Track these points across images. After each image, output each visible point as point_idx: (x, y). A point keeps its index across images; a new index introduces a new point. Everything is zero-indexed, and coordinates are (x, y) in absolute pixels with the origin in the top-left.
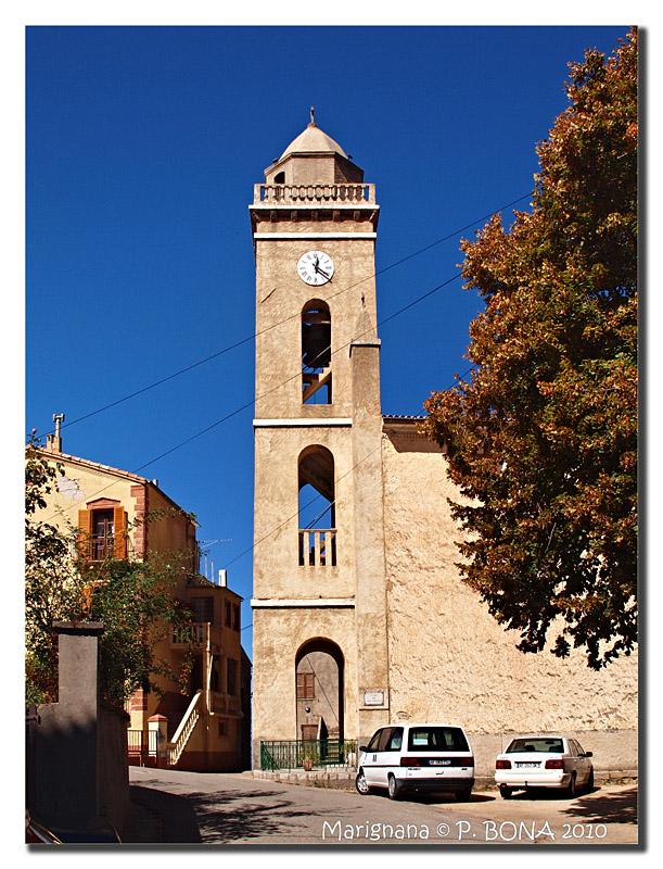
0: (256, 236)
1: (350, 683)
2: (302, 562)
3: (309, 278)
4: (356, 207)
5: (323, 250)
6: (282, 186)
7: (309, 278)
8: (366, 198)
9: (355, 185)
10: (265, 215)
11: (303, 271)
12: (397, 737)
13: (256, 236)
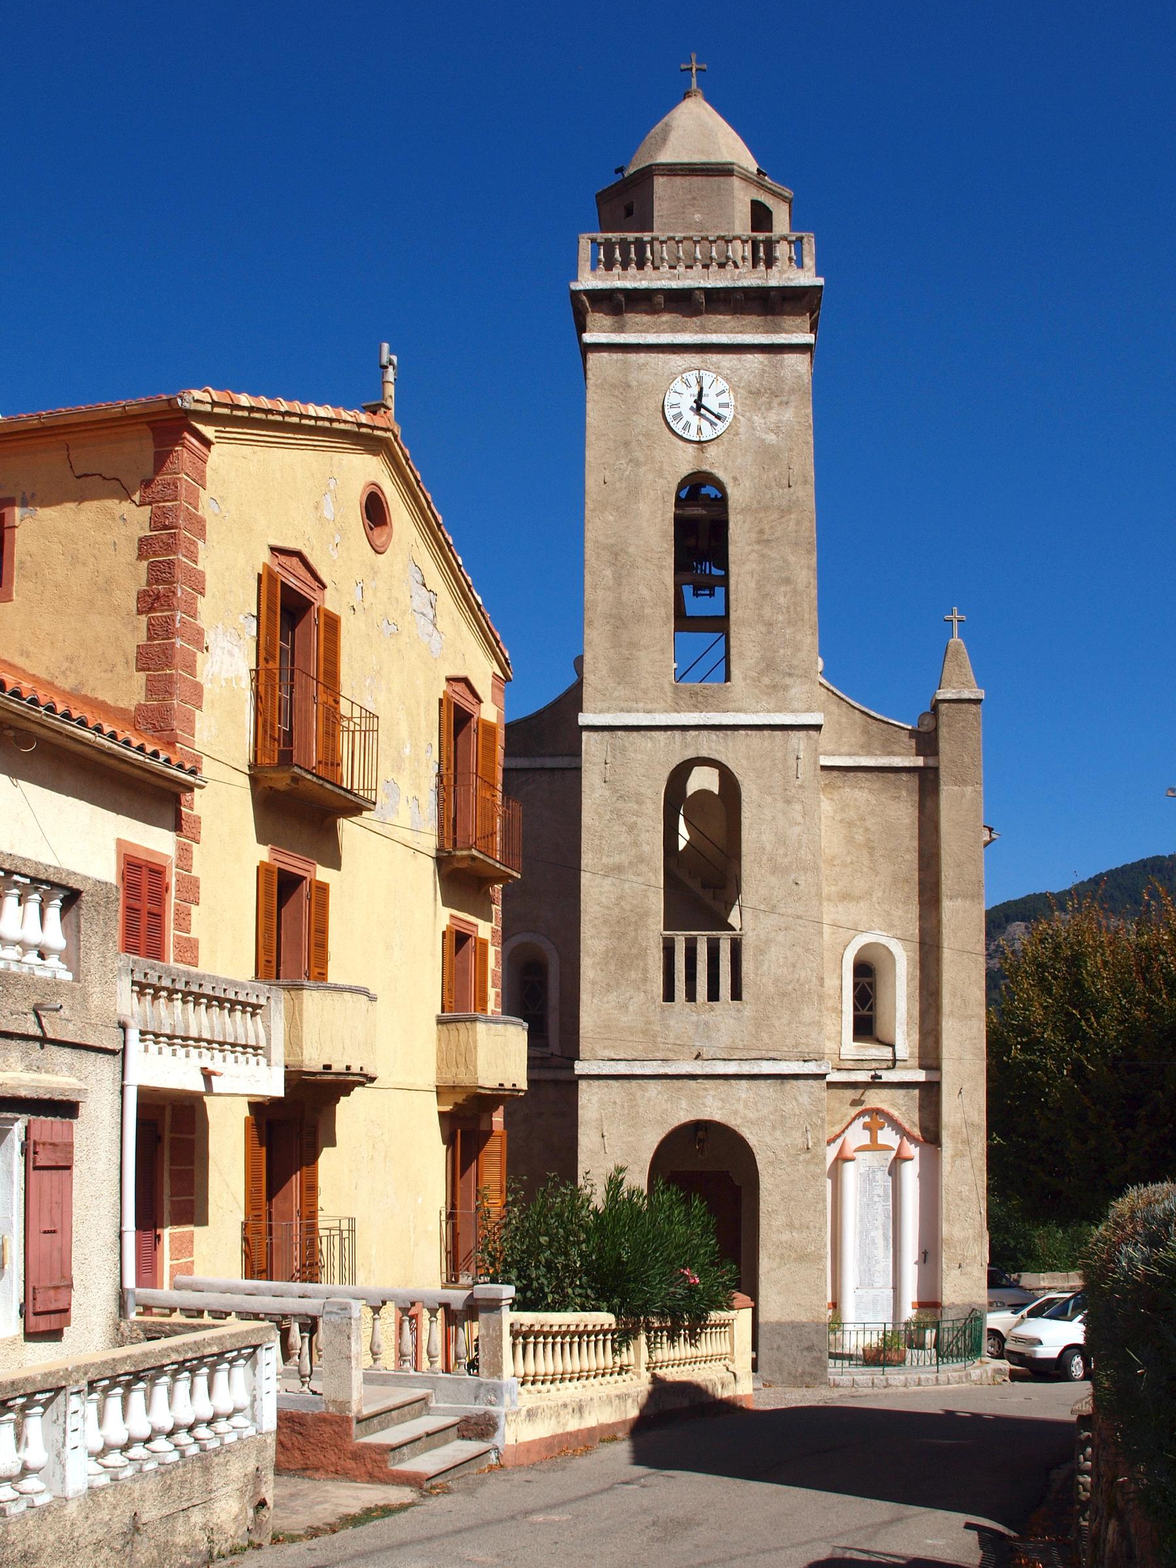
0: (588, 338)
1: (886, 1257)
2: (669, 995)
3: (678, 417)
4: (619, 284)
5: (718, 371)
6: (647, 236)
7: (678, 417)
8: (800, 265)
9: (631, 236)
10: (617, 303)
11: (675, 411)
12: (308, 1165)
13: (588, 338)
